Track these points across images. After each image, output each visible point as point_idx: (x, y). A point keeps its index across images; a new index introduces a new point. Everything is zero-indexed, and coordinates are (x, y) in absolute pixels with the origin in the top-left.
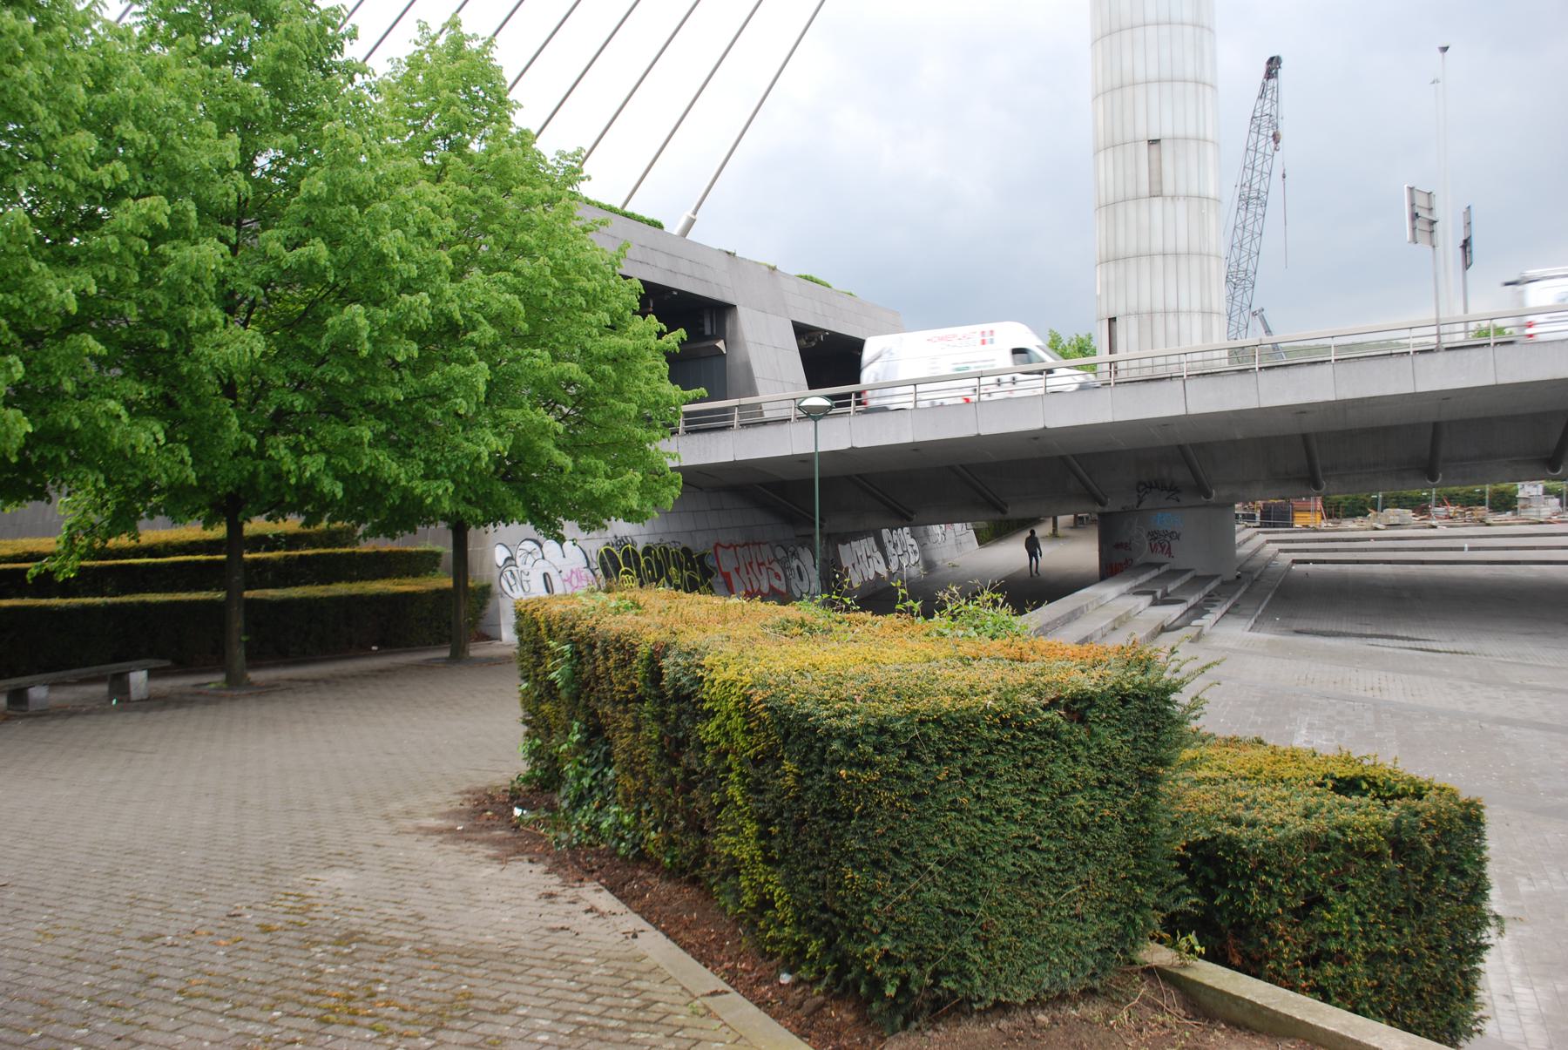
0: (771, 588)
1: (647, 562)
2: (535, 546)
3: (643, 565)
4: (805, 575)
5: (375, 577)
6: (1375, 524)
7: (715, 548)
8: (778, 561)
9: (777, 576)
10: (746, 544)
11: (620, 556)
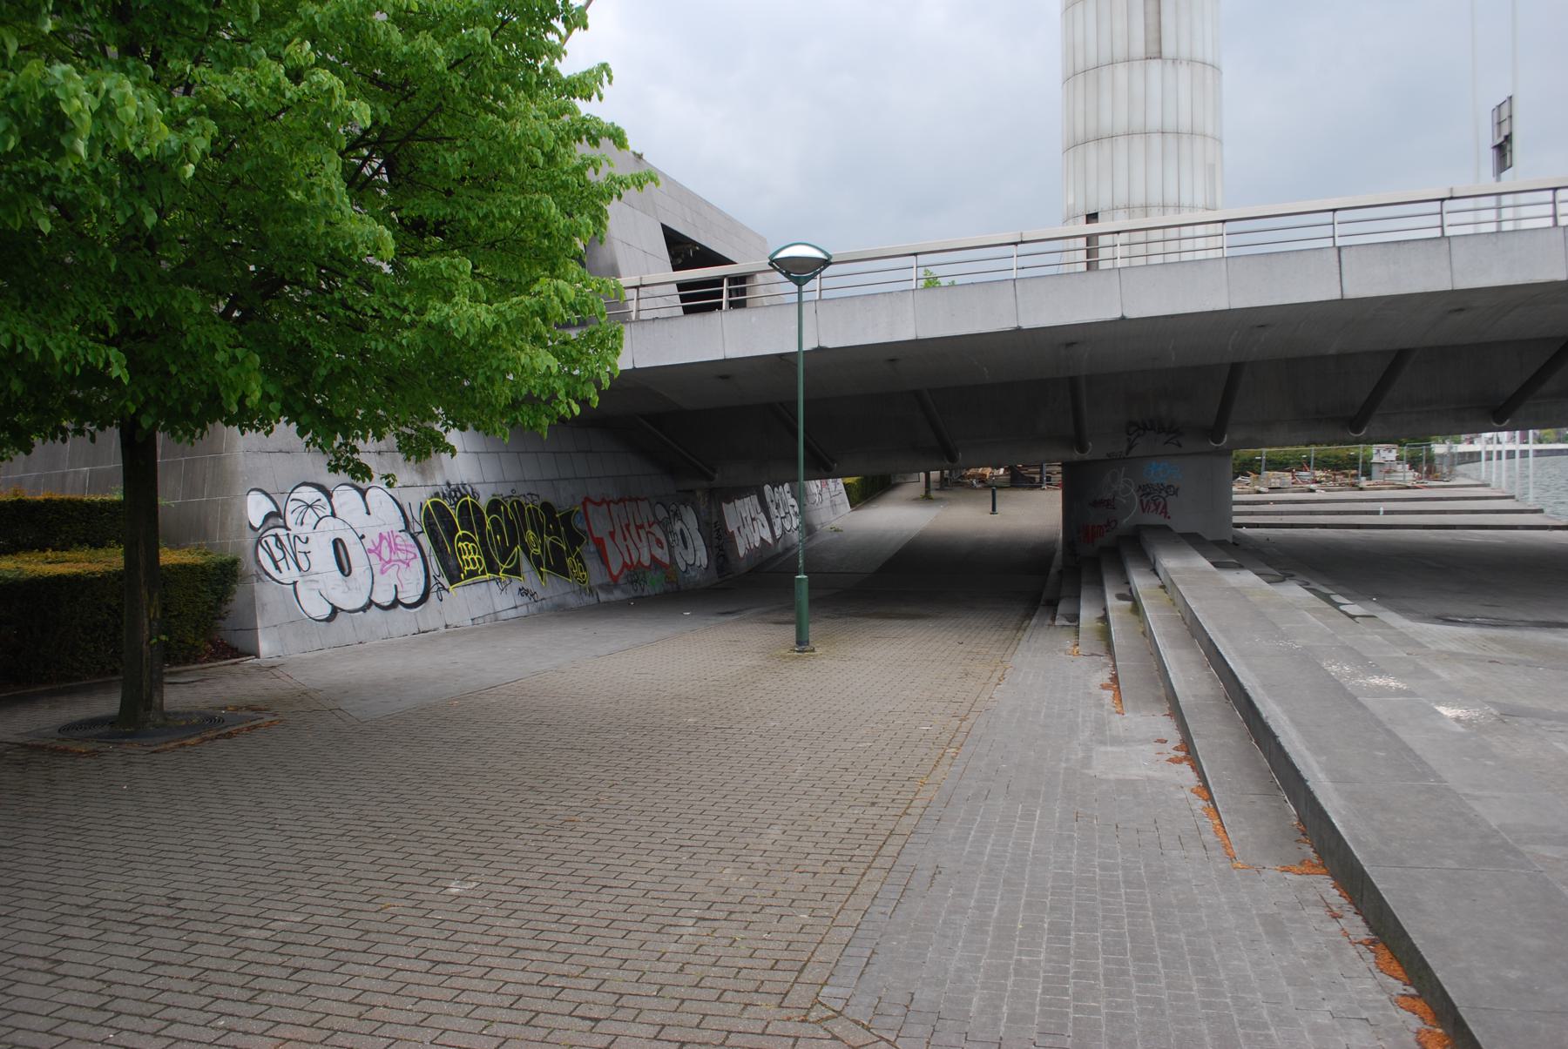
0: (653, 558)
1: (495, 522)
2: (320, 495)
3: (488, 527)
4: (689, 542)
5: (39, 545)
6: (1257, 487)
7: (584, 504)
8: (659, 523)
9: (659, 542)
10: (621, 500)
11: (454, 513)
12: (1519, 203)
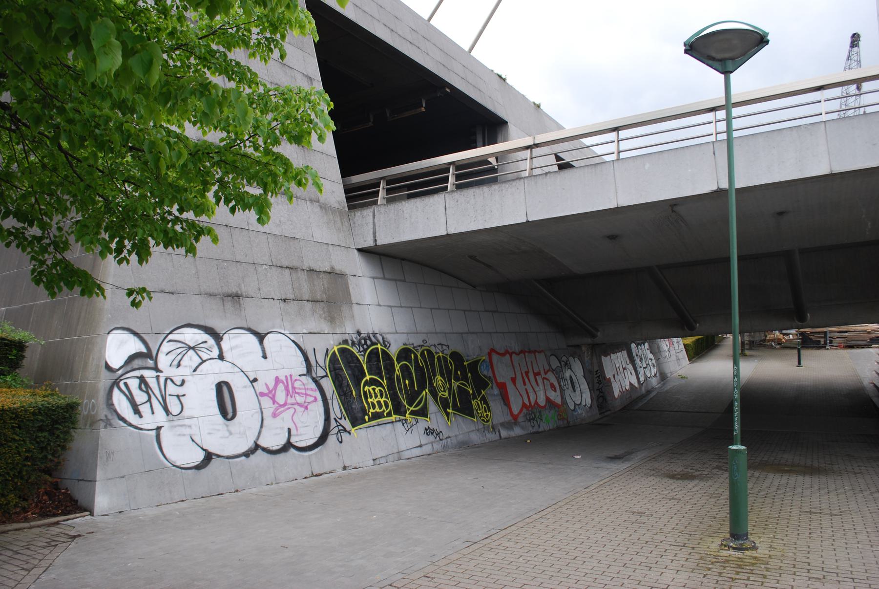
4: (577, 386)
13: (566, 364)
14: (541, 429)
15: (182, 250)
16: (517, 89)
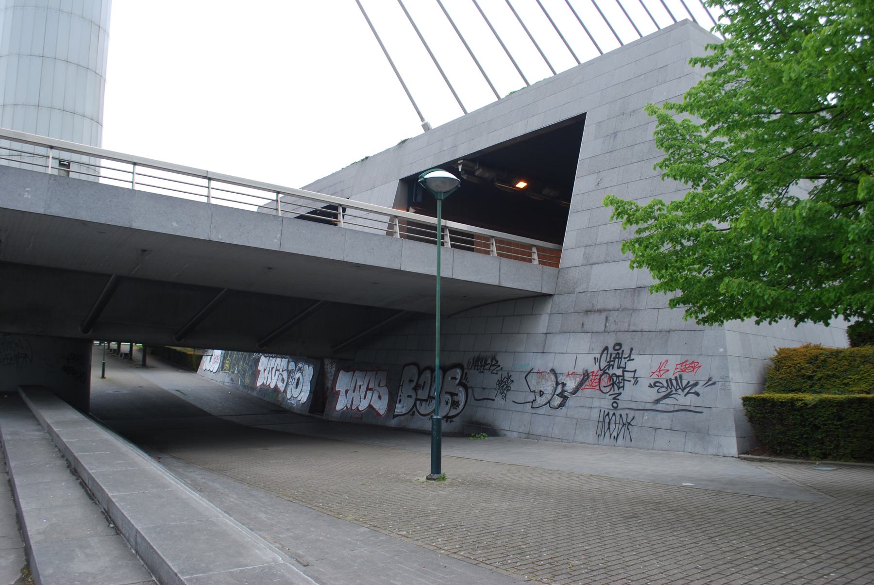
4: (300, 386)
9: (283, 380)
12: (36, 152)
13: (300, 369)
14: (265, 399)
15: (717, 324)
16: (339, 169)
